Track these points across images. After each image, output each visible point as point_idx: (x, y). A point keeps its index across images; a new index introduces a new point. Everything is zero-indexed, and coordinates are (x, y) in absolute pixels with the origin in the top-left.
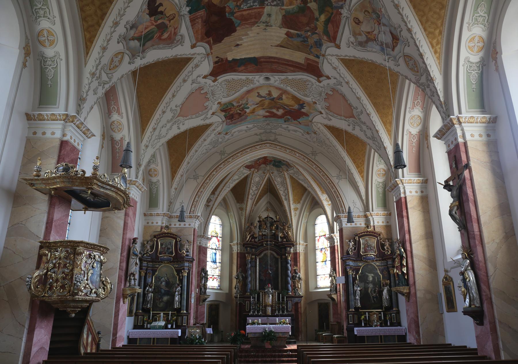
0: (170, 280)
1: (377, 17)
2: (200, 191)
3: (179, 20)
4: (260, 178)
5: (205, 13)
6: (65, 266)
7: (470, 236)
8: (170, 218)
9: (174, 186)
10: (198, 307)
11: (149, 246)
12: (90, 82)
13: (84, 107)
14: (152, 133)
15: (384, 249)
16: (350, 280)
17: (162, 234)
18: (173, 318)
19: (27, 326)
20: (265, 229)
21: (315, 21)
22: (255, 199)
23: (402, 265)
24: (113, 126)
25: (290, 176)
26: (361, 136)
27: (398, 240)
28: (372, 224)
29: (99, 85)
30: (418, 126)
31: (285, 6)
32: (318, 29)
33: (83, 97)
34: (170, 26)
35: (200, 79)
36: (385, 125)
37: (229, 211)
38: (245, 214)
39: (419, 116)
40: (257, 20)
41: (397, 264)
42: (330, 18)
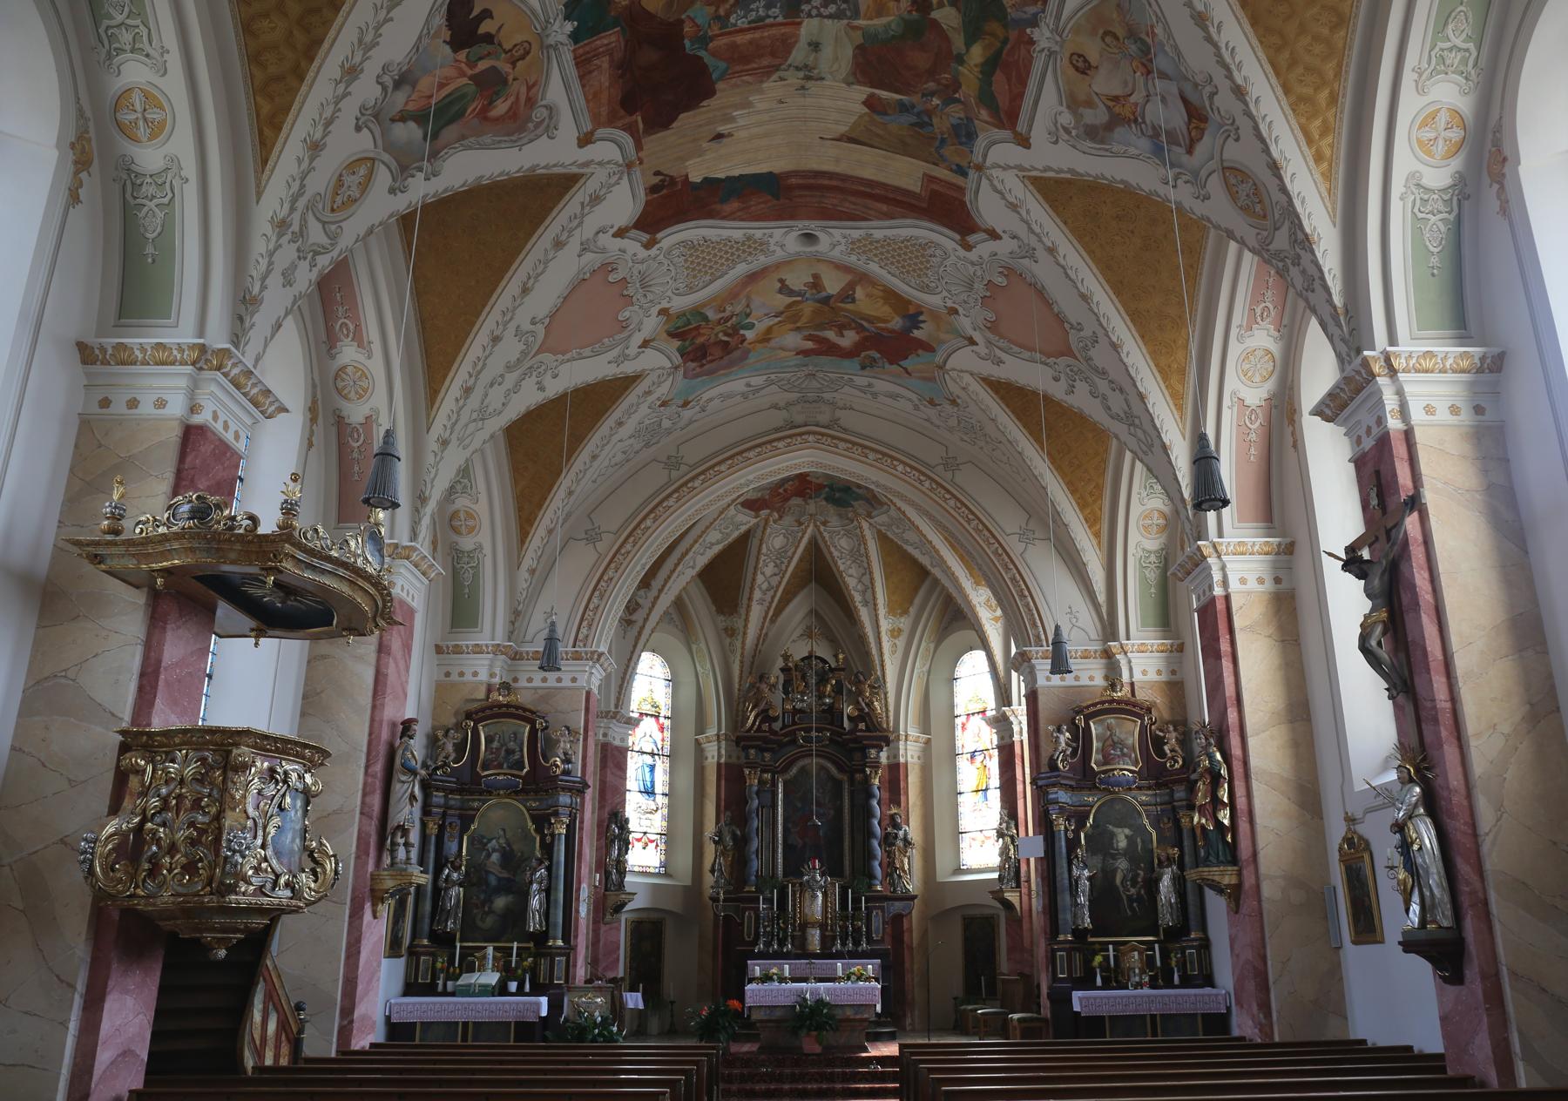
0: (515, 847)
1: (1142, 51)
2: (606, 578)
3: (543, 60)
4: (788, 539)
5: (621, 39)
6: (196, 805)
7: (1423, 714)
8: (514, 659)
9: (527, 562)
10: (599, 929)
11: (451, 745)
12: (271, 247)
13: (253, 325)
14: (461, 402)
15: (1162, 754)
16: (1061, 848)
17: (491, 708)
18: (525, 963)
19: (81, 986)
20: (803, 694)
21: (952, 64)
22: (771, 603)
23: (1216, 803)
24: (343, 380)
25: (879, 532)
26: (1094, 410)
27: (1205, 727)
28: (1125, 677)
29: (299, 258)
30: (1265, 380)
31: (864, 19)
32: (963, 87)
33: (251, 293)
34: (514, 80)
35: (606, 240)
36: (1165, 378)
37: (694, 638)
38: (743, 648)
39: (1268, 352)
40: (777, 61)
41: (1202, 798)
42: (999, 53)
